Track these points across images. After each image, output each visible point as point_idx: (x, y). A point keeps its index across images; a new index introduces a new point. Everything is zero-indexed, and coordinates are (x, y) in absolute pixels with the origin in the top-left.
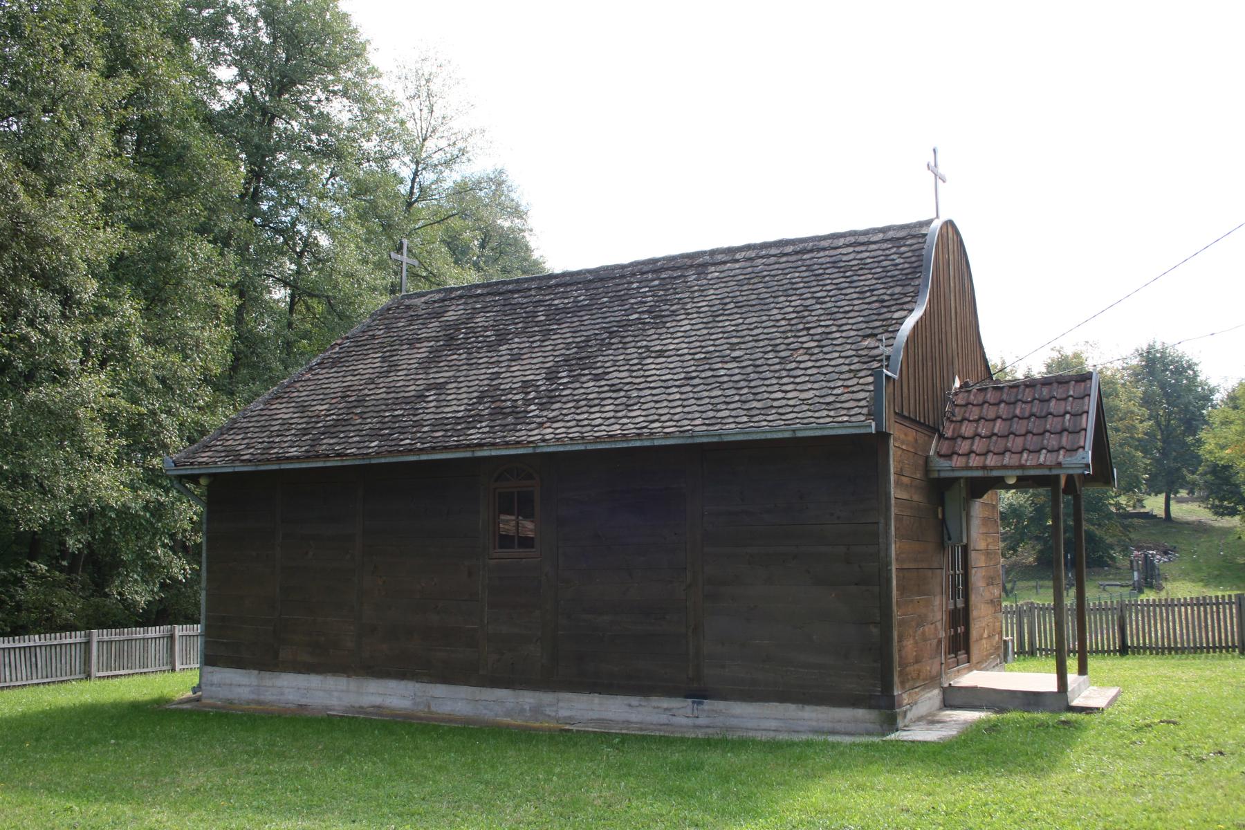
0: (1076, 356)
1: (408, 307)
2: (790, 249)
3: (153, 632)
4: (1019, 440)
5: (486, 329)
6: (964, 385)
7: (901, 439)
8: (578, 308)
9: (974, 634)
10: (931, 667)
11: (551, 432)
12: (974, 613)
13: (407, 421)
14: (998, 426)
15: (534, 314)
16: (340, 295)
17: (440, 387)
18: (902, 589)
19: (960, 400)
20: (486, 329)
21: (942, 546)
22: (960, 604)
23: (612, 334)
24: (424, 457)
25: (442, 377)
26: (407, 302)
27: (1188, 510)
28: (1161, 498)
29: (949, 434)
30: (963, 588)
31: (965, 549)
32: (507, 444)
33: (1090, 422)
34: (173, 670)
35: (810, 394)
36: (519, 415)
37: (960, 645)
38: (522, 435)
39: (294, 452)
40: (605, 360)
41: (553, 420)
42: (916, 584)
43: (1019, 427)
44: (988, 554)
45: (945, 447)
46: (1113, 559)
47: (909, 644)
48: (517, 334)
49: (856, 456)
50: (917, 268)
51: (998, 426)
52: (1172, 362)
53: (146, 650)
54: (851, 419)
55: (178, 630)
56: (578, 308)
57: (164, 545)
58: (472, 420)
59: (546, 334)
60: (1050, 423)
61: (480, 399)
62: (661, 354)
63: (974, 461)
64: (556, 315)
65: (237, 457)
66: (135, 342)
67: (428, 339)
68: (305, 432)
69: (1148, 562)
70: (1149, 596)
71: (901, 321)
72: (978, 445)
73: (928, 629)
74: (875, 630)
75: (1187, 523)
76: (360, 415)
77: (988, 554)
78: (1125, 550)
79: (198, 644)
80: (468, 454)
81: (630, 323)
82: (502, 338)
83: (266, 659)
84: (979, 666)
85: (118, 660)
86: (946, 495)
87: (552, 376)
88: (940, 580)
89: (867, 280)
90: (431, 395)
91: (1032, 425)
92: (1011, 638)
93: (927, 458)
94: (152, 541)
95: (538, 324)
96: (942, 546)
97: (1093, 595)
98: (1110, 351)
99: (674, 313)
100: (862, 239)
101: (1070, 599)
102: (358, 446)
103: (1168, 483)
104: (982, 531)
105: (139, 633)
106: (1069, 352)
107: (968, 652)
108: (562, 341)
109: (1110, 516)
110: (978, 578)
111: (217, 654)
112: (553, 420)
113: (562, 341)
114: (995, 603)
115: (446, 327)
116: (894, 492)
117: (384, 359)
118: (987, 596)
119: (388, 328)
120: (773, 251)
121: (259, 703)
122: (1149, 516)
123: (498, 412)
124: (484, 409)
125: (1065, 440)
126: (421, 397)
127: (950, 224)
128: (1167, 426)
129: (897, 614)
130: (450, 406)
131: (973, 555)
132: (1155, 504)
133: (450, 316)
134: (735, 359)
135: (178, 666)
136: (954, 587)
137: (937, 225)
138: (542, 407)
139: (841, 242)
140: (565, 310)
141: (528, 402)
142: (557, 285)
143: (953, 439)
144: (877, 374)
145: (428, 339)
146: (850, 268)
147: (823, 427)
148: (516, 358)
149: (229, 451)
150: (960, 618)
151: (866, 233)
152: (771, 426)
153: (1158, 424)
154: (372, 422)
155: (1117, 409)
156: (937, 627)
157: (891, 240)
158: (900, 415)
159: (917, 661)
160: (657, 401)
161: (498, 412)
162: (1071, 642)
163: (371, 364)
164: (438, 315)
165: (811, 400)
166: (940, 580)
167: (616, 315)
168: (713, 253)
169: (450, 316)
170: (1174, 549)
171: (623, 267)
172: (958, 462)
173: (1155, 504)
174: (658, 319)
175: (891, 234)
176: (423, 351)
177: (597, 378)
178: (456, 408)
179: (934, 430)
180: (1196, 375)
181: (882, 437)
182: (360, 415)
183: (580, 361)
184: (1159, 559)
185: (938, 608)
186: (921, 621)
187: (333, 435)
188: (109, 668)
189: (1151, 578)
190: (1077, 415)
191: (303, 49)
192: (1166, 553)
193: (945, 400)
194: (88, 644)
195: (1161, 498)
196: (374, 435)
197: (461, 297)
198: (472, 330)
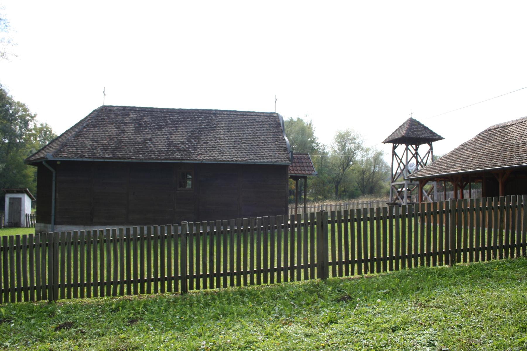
5: (151, 123)
24: (163, 161)
80: (179, 161)
100: (259, 114)
102: (129, 155)
147: (280, 162)
157: (266, 116)
168: (216, 110)
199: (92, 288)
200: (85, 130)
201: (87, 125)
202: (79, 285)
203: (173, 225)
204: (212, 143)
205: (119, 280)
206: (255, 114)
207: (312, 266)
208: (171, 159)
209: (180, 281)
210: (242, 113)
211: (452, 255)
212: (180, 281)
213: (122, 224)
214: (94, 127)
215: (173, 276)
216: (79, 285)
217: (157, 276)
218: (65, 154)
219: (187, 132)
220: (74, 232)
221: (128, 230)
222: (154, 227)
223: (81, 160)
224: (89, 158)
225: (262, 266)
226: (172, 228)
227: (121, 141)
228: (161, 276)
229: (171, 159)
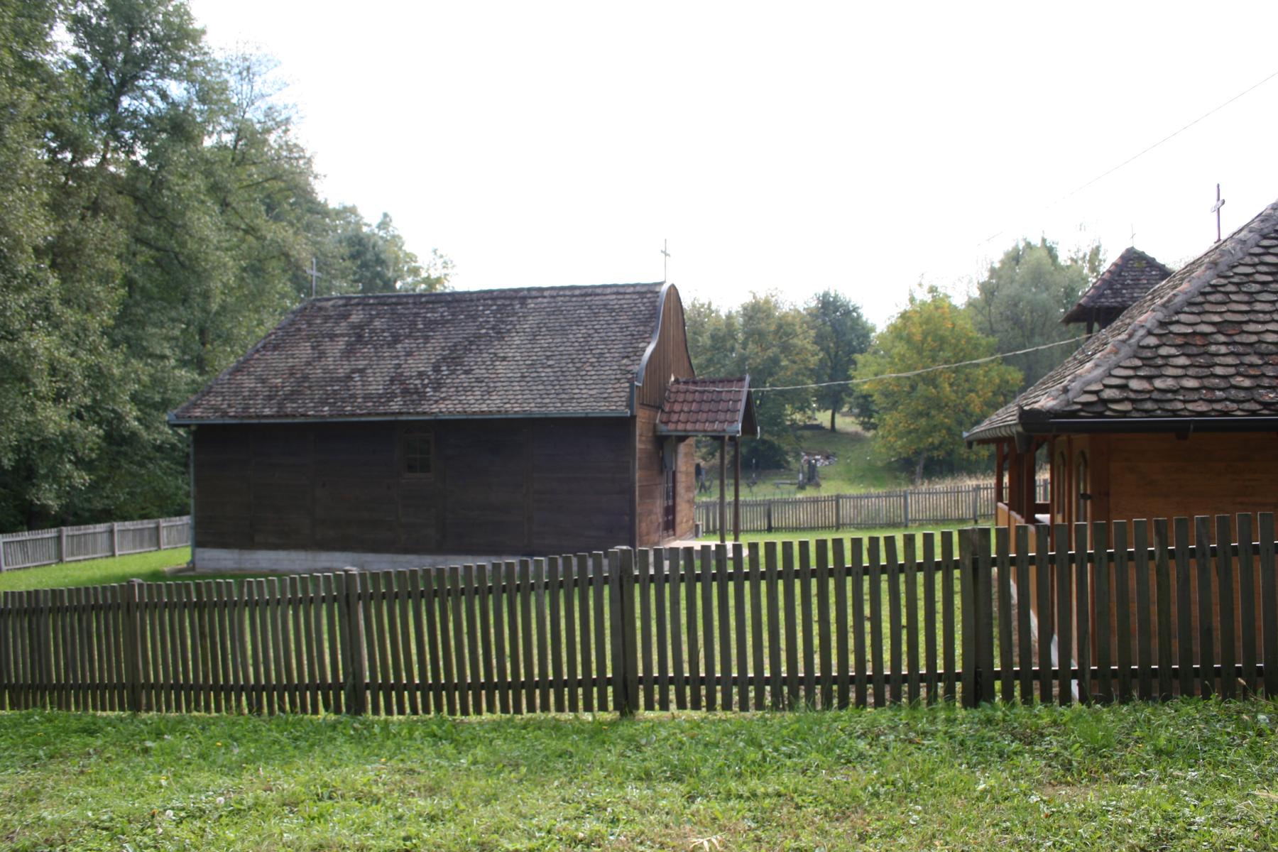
0: (767, 302)
1: (320, 309)
2: (577, 292)
3: (101, 527)
4: (705, 415)
5: (383, 331)
6: (677, 381)
7: (642, 416)
8: (445, 322)
9: (678, 520)
10: (654, 537)
11: (444, 406)
12: (678, 508)
13: (344, 394)
14: (694, 406)
15: (414, 323)
16: (186, 252)
17: (361, 371)
18: (641, 496)
19: (674, 390)
20: (383, 331)
21: (661, 472)
22: (671, 503)
23: (471, 343)
24: (363, 419)
25: (361, 364)
26: (319, 304)
27: (846, 423)
28: (829, 413)
29: (667, 409)
30: (672, 494)
31: (674, 473)
32: (418, 413)
33: (741, 406)
34: (113, 555)
35: (594, 392)
36: (422, 396)
37: (670, 526)
38: (426, 408)
39: (267, 411)
40: (469, 359)
41: (444, 399)
42: (648, 494)
43: (705, 407)
44: (687, 474)
45: (665, 418)
46: (788, 462)
47: (644, 525)
48: (407, 337)
49: (618, 428)
50: (653, 314)
51: (694, 406)
52: (842, 306)
53: (95, 540)
54: (615, 406)
55: (117, 526)
56: (445, 322)
57: (70, 461)
58: (391, 397)
59: (427, 339)
60: (722, 406)
61: (392, 381)
62: (504, 359)
63: (680, 427)
64: (430, 324)
65: (225, 414)
66: (56, 303)
67: (342, 335)
68: (270, 398)
69: (812, 468)
70: (810, 492)
71: (644, 350)
72: (683, 417)
73: (654, 517)
74: (626, 518)
75: (847, 434)
76: (309, 387)
77: (687, 474)
78: (797, 456)
79: (188, 534)
80: (393, 418)
81: (479, 337)
82: (396, 339)
83: (247, 542)
84: (680, 538)
85: (81, 546)
86: (664, 444)
87: (437, 369)
88: (660, 491)
89: (624, 319)
90: (356, 376)
91: (712, 406)
92: (701, 523)
93: (655, 425)
94: (61, 457)
95: (419, 330)
96: (661, 472)
97: (745, 495)
98: (796, 296)
99: (509, 331)
100: (622, 290)
101: (729, 497)
102: (311, 409)
103: (833, 400)
104: (685, 461)
105: (91, 529)
106: (761, 296)
107: (674, 530)
108: (437, 345)
109: (785, 429)
110: (681, 489)
111: (203, 538)
112: (444, 399)
113: (437, 345)
114: (691, 502)
115: (353, 327)
116: (639, 446)
117: (313, 348)
118: (686, 498)
119: (310, 325)
120: (568, 293)
121: (240, 570)
122: (819, 428)
123: (406, 392)
124: (396, 388)
125: (729, 416)
126: (349, 377)
127: (673, 287)
128: (836, 355)
129: (638, 509)
130: (371, 383)
131: (679, 475)
132: (823, 418)
133: (355, 318)
134: (550, 366)
135: (117, 553)
136: (668, 493)
137: (664, 288)
138: (435, 390)
139: (609, 291)
140: (436, 322)
141: (425, 386)
142: (427, 302)
143: (669, 413)
144: (631, 381)
145: (342, 335)
146: (613, 310)
147: (602, 411)
148: (409, 354)
149: (216, 409)
150: (671, 511)
151: (623, 286)
152: (574, 409)
153: (828, 353)
154: (318, 394)
155: (795, 346)
156: (658, 517)
157: (638, 293)
158: (642, 404)
159: (648, 534)
160: (501, 387)
161: (406, 392)
162: (729, 524)
163: (304, 351)
164: (346, 316)
165: (595, 395)
166: (660, 491)
167: (471, 329)
168: (529, 290)
169: (355, 318)
170: (834, 455)
171: (470, 293)
172: (671, 426)
173: (823, 418)
174: (500, 336)
175: (638, 289)
176: (341, 344)
177: (467, 372)
178: (377, 387)
179: (659, 408)
180: (859, 317)
181: (633, 417)
182: (309, 387)
183: (453, 359)
184: (820, 462)
185: (659, 505)
186: (650, 513)
187: (293, 401)
188: (73, 555)
189: (812, 478)
190: (736, 401)
191: (138, 32)
192: (827, 458)
193: (665, 389)
194: (59, 538)
195: (829, 413)
196: (324, 402)
197: (358, 304)
198: (373, 331)
199: (580, 691)
200: (257, 356)
201: (264, 347)
202: (594, 683)
203: (591, 555)
204: (478, 372)
205: (580, 677)
206: (615, 290)
207: (950, 677)
208: (378, 414)
209: (610, 689)
210: (584, 291)
211: (353, 695)
212: (610, 689)
213: (513, 553)
214: (275, 348)
215: (940, 671)
216: (594, 683)
217: (864, 670)
218: (197, 412)
219: (443, 349)
220: (466, 567)
221: (524, 565)
222: (550, 559)
223: (220, 421)
224: (235, 417)
225: (718, 668)
226: (590, 562)
227: (306, 378)
228: (722, 671)
229: (378, 414)
